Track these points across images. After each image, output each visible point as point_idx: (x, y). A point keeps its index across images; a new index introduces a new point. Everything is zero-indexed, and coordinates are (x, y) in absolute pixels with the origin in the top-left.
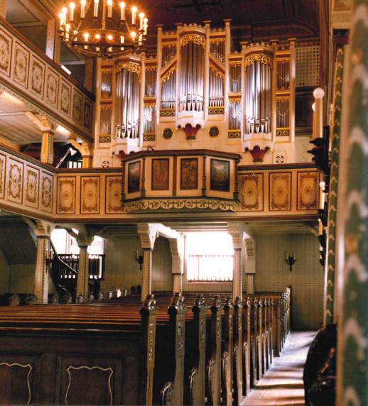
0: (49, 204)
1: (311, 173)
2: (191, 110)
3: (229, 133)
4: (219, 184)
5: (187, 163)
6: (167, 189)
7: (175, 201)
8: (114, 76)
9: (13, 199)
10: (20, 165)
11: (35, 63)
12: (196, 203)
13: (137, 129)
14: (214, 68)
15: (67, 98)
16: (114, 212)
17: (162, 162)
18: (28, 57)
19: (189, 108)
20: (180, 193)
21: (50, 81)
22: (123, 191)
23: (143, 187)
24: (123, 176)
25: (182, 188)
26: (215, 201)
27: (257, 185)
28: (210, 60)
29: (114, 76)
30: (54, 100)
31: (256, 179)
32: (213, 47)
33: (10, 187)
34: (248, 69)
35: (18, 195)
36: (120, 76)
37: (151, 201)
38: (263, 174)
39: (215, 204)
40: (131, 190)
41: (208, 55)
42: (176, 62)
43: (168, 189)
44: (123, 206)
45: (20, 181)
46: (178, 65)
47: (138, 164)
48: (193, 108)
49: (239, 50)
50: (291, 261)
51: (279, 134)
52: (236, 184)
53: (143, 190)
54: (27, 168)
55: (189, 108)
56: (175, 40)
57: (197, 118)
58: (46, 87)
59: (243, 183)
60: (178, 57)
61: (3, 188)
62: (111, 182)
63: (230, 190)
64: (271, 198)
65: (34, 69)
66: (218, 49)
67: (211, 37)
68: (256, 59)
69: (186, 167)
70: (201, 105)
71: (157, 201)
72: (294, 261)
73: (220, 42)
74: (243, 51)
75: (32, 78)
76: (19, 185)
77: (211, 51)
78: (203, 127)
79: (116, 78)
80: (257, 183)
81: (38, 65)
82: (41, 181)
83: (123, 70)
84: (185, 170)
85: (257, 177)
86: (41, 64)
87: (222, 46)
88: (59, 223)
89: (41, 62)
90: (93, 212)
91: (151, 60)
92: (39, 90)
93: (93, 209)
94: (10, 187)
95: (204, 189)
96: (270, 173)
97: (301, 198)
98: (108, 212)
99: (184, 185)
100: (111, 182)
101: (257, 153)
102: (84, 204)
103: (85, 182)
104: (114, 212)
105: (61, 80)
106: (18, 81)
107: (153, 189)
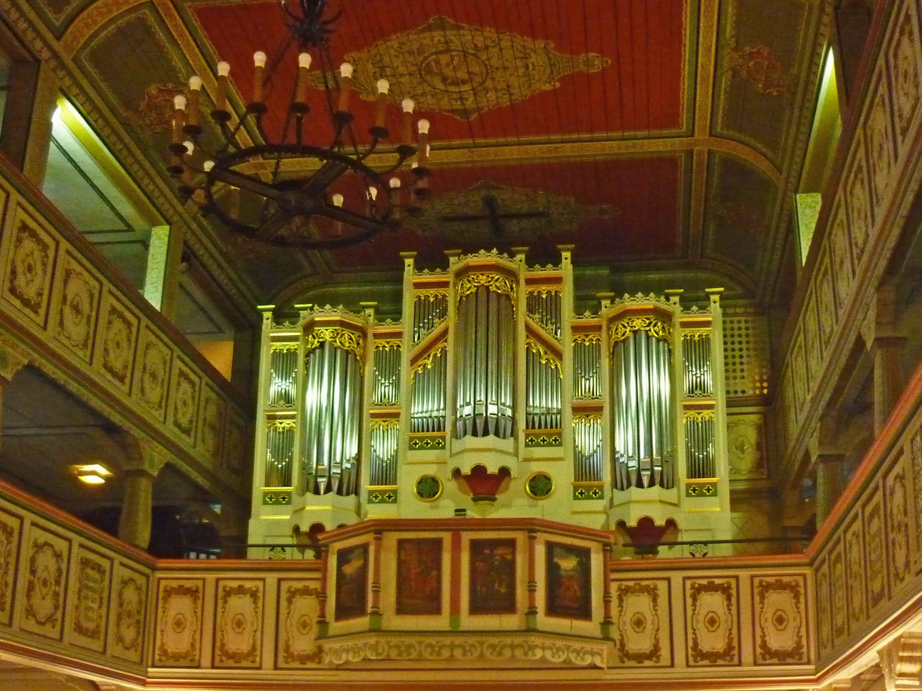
1: (644, 583)
3: (576, 488)
6: (436, 610)
7: (459, 640)
8: (301, 360)
9: (37, 629)
11: (182, 374)
13: (353, 477)
15: (190, 401)
18: (168, 358)
20: (468, 622)
21: (148, 357)
22: (323, 615)
24: (324, 580)
25: (476, 609)
26: (560, 643)
28: (528, 328)
29: (301, 360)
30: (157, 400)
31: (652, 593)
32: (533, 304)
34: (618, 350)
35: (51, 619)
36: (315, 359)
37: (394, 641)
38: (669, 580)
39: (559, 649)
42: (446, 332)
45: (58, 583)
46: (451, 337)
48: (491, 428)
49: (596, 310)
51: (695, 491)
53: (376, 614)
56: (445, 284)
57: (490, 453)
58: (201, 423)
61: (8, 600)
63: (519, 606)
64: (690, 636)
65: (179, 384)
66: (548, 308)
67: (529, 282)
70: (509, 424)
73: (549, 292)
75: (175, 404)
77: (531, 310)
78: (514, 474)
79: (307, 364)
80: (655, 600)
81: (187, 378)
82: (116, 587)
83: (322, 345)
85: (655, 588)
86: (193, 377)
87: (555, 301)
89: (195, 373)
91: (388, 327)
92: (121, 373)
96: (685, 579)
98: (281, 663)
100: (293, 594)
101: (647, 536)
102: (223, 645)
104: (296, 665)
106: (66, 342)
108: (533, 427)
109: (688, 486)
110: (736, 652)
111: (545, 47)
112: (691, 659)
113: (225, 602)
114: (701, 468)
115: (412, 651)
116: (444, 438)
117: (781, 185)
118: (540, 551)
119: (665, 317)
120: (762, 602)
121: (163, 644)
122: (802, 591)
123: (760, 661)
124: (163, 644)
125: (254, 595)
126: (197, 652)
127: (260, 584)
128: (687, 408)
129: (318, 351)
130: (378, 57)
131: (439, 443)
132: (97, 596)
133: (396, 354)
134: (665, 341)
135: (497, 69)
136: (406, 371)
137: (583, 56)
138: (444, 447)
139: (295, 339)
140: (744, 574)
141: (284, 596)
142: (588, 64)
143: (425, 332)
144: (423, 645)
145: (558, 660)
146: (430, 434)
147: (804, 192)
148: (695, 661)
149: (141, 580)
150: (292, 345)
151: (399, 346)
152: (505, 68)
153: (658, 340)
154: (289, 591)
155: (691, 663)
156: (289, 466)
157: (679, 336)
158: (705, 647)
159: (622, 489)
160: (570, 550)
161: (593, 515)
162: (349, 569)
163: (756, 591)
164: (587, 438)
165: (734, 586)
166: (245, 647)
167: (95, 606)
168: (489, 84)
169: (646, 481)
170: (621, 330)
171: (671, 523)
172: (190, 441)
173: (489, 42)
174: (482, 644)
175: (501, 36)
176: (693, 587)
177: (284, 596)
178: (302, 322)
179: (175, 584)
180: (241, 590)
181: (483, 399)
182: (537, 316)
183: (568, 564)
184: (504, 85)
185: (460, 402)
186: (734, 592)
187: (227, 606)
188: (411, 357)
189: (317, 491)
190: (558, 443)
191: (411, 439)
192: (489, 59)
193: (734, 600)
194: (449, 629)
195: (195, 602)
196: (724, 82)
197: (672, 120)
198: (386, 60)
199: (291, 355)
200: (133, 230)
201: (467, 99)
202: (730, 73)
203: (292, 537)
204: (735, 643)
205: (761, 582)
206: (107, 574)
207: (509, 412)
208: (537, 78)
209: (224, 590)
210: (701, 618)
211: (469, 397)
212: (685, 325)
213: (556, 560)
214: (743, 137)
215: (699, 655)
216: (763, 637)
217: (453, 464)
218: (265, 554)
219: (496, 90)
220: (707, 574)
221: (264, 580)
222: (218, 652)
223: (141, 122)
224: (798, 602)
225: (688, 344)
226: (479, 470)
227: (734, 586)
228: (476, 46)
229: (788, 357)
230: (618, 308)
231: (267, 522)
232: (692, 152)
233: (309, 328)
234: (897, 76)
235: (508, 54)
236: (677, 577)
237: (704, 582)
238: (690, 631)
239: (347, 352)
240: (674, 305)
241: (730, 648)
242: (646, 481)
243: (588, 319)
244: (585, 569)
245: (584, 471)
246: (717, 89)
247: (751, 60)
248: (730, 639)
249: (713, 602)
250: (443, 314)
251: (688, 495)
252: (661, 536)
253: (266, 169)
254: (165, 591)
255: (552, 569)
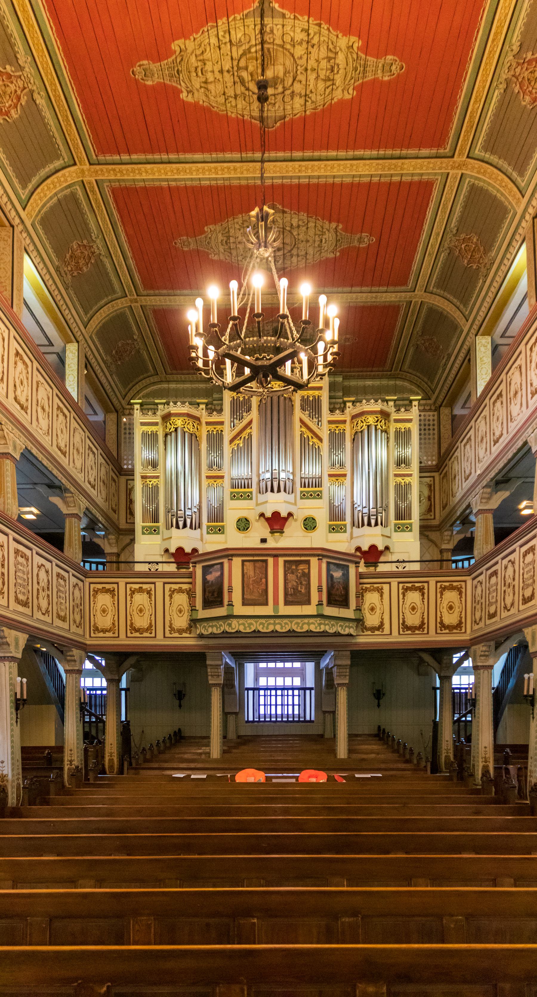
0: (47, 611)
1: (376, 586)
2: (279, 491)
4: (337, 598)
5: (294, 567)
7: (277, 621)
10: (48, 565)
12: (309, 624)
14: (308, 434)
16: (177, 635)
17: (258, 565)
19: (276, 489)
23: (230, 600)
24: (193, 583)
25: (287, 603)
27: (382, 599)
28: (301, 421)
31: (380, 591)
33: (38, 598)
34: (357, 437)
37: (241, 621)
39: (333, 625)
40: (208, 603)
41: (298, 413)
42: (250, 422)
43: (266, 604)
44: (191, 627)
46: (254, 425)
47: (219, 566)
50: (180, 696)
51: (398, 528)
52: (357, 597)
53: (231, 605)
54: (56, 570)
55: (276, 489)
57: (276, 503)
59: (363, 596)
60: (254, 414)
62: (172, 592)
68: (371, 422)
69: (293, 573)
71: (250, 621)
72: (184, 695)
74: (347, 411)
75: (15, 382)
76: (48, 596)
80: (381, 596)
83: (176, 430)
84: (290, 576)
85: (382, 589)
88: (89, 651)
90: (145, 635)
91: (215, 418)
93: (147, 630)
94: (38, 598)
95: (320, 604)
97: (441, 617)
99: (290, 598)
100: (172, 592)
101: (372, 555)
102: (132, 624)
103: (133, 592)
104: (177, 635)
105: (87, 440)
107: (244, 604)
108: (305, 487)
109: (396, 525)
110: (463, 625)
111: (336, 228)
112: (401, 630)
113: (132, 597)
114: (402, 514)
115: (252, 626)
116: (251, 493)
117: (466, 330)
118: (324, 566)
119: (385, 415)
120: (441, 597)
121: (95, 624)
122: (464, 590)
123: (439, 631)
124: (95, 624)
125: (149, 592)
126: (117, 628)
127: (115, 586)
128: (396, 475)
129: (173, 434)
130: (227, 230)
131: (248, 496)
132: (64, 596)
133: (220, 435)
134: (386, 432)
135: (302, 241)
136: (227, 448)
137: (358, 236)
138: (251, 499)
139: (156, 424)
140: (432, 581)
141: (167, 593)
142: (360, 240)
143: (238, 421)
144: (258, 623)
145: (331, 631)
146: (243, 490)
147: (481, 335)
148: (403, 631)
149: (80, 584)
150: (154, 428)
151: (222, 431)
152: (307, 241)
153: (382, 431)
154: (170, 590)
155: (401, 632)
156: (157, 509)
157: (393, 427)
158: (409, 623)
159: (359, 527)
160: (338, 566)
161: (341, 543)
162: (210, 578)
163: (438, 590)
164: (338, 493)
165: (426, 587)
166: (145, 625)
167: (64, 602)
168: (295, 252)
169: (373, 522)
170: (360, 424)
171: (387, 548)
172: (95, 492)
173: (301, 223)
174: (291, 622)
175: (310, 219)
176: (403, 588)
177: (167, 593)
178: (159, 413)
179: (100, 586)
180: (141, 590)
181: (277, 468)
182: (307, 412)
183: (337, 574)
184: (303, 253)
185: (262, 470)
186: (426, 591)
187: (133, 599)
188: (230, 439)
189: (178, 527)
190: (319, 496)
191: (231, 493)
192: (298, 234)
193: (426, 596)
194: (316, 614)
195: (113, 597)
196: (443, 256)
197: (403, 281)
198: (232, 231)
199: (154, 435)
200: (53, 345)
201: (278, 262)
202: (448, 251)
203: (162, 555)
204: (426, 621)
205: (441, 586)
206: (67, 581)
207: (291, 477)
208: (326, 249)
209: (131, 590)
210: (407, 606)
211: (268, 467)
212: (396, 421)
213: (331, 572)
214: (446, 294)
215: (406, 627)
216: (441, 617)
217: (260, 510)
218: (144, 568)
219: (298, 256)
220: (410, 581)
221: (117, 583)
222: (129, 628)
223: (66, 269)
224: (461, 597)
225: (398, 433)
226: (276, 514)
227: (426, 587)
228: (292, 225)
229: (458, 443)
230: (359, 408)
231: (148, 548)
232: (411, 302)
233: (166, 418)
234: (531, 362)
235: (311, 232)
236: (394, 582)
237: (409, 585)
238: (401, 614)
239: (191, 434)
240: (390, 408)
241: (423, 623)
242: (373, 522)
243: (337, 416)
244: (346, 576)
245: (336, 514)
246: (437, 260)
247: (463, 243)
248: (423, 619)
249: (414, 597)
250: (249, 410)
251: (396, 531)
252: (379, 557)
253: (137, 302)
254: (94, 591)
255: (330, 577)
